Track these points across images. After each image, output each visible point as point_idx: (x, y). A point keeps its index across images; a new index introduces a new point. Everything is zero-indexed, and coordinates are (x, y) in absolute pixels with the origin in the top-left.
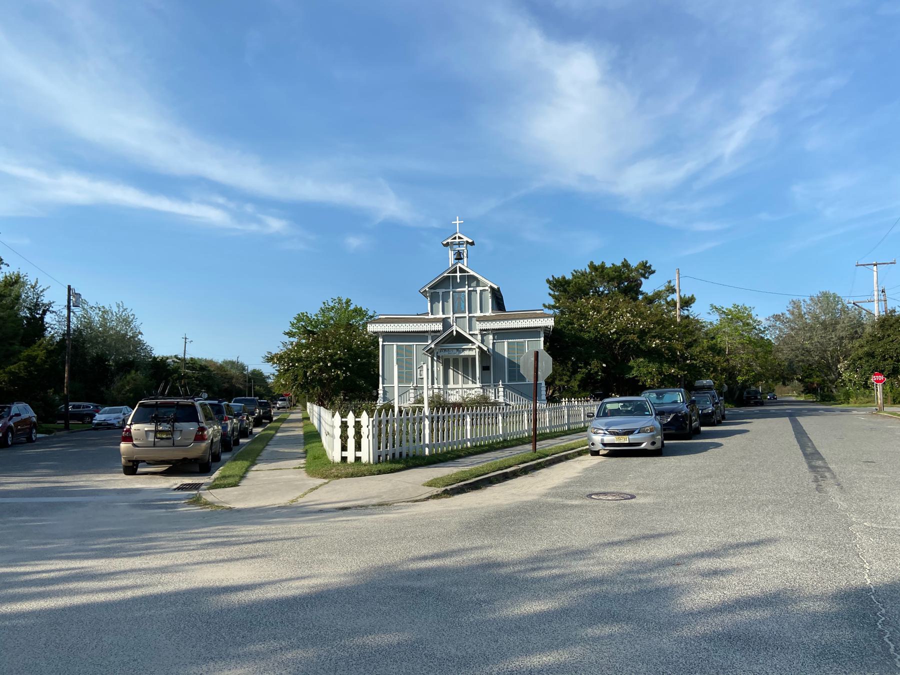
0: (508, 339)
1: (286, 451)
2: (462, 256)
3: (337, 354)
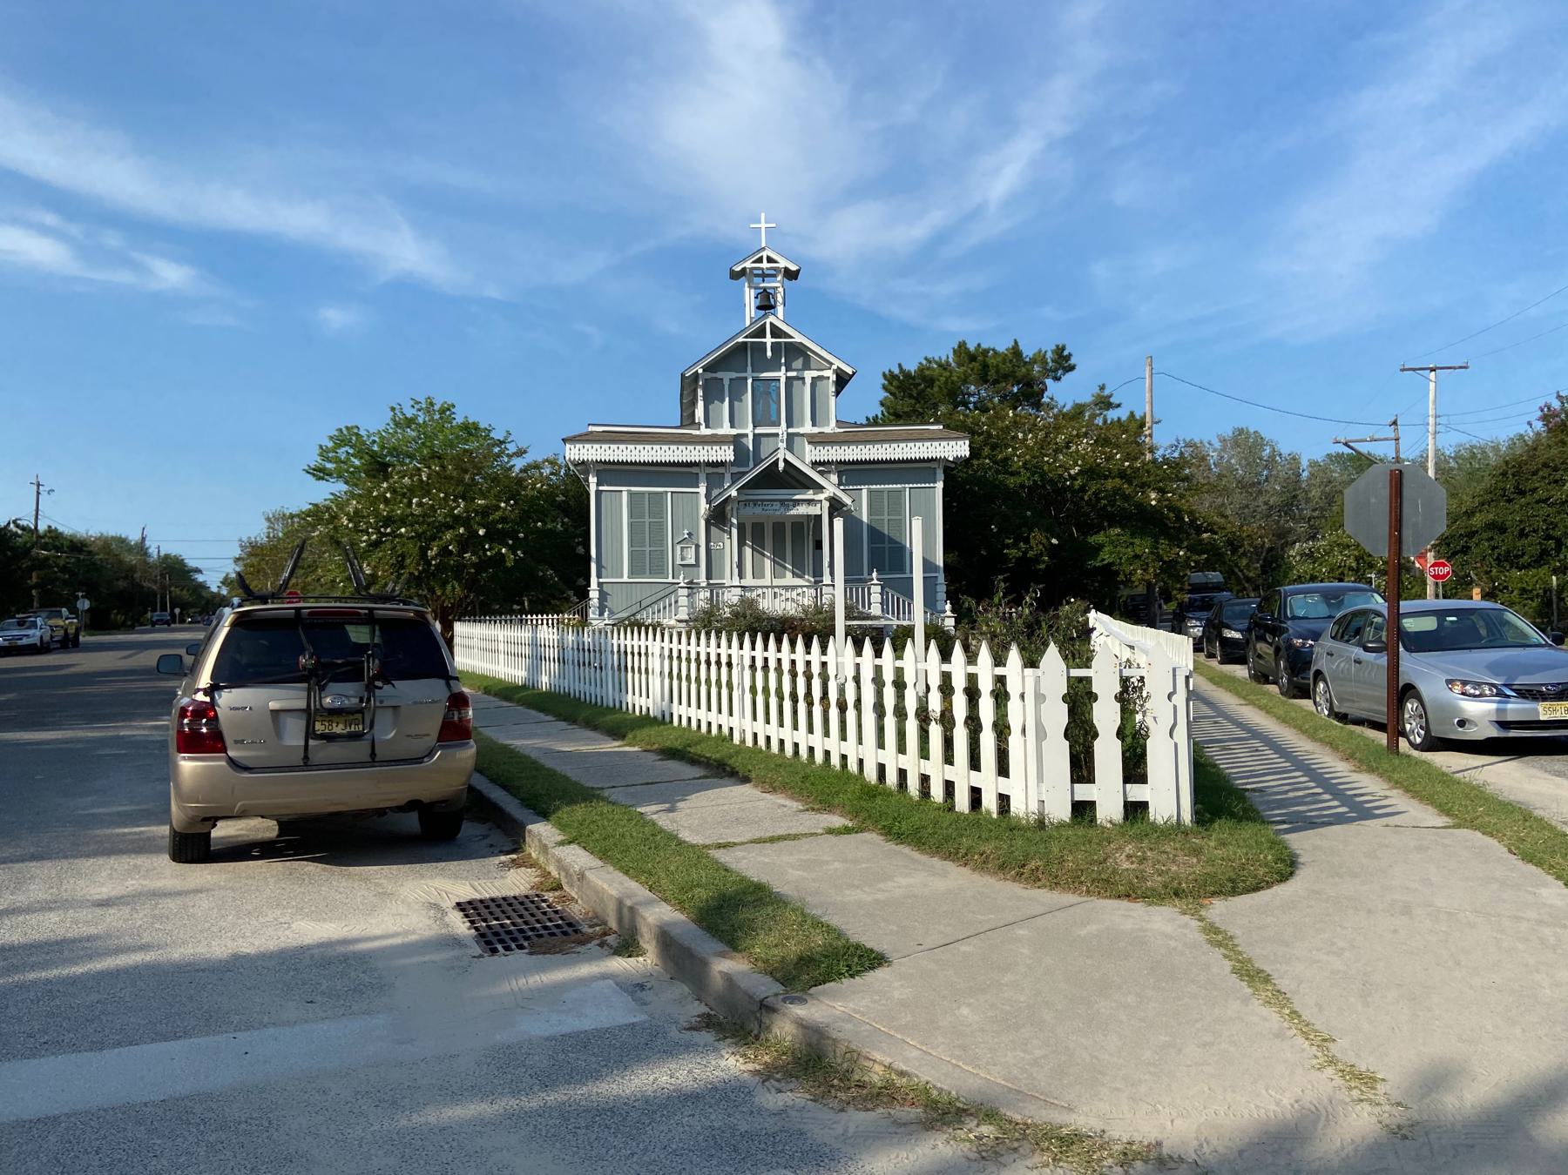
1: (584, 749)
2: (772, 301)
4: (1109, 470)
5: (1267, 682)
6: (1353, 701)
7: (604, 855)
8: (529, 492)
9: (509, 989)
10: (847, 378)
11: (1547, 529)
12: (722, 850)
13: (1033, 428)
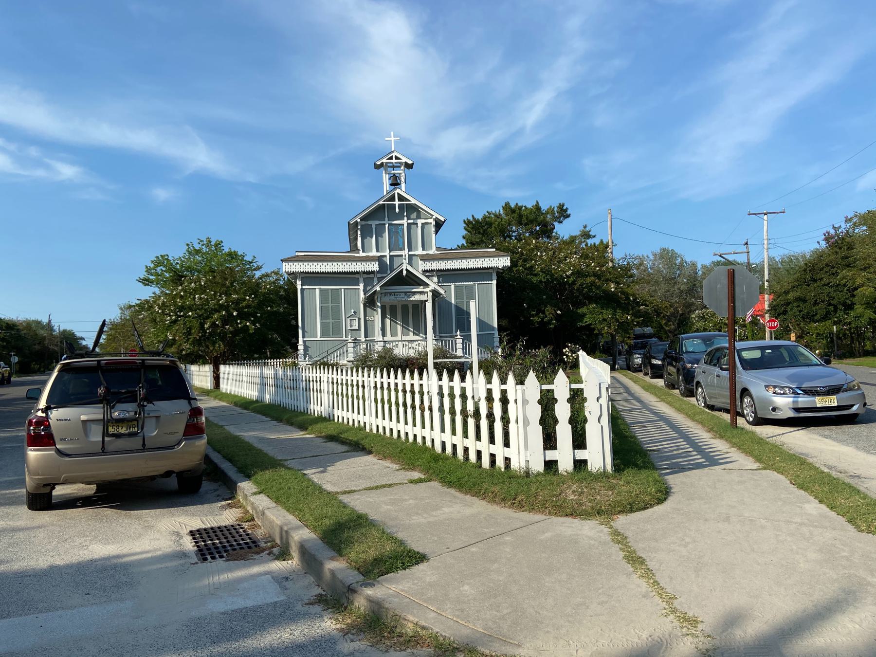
0: (455, 282)
1: (282, 437)
2: (399, 181)
3: (245, 299)
4: (588, 272)
5: (674, 388)
6: (717, 398)
7: (277, 500)
8: (263, 291)
9: (207, 583)
10: (442, 223)
11: (829, 300)
12: (347, 495)
13: (546, 250)
